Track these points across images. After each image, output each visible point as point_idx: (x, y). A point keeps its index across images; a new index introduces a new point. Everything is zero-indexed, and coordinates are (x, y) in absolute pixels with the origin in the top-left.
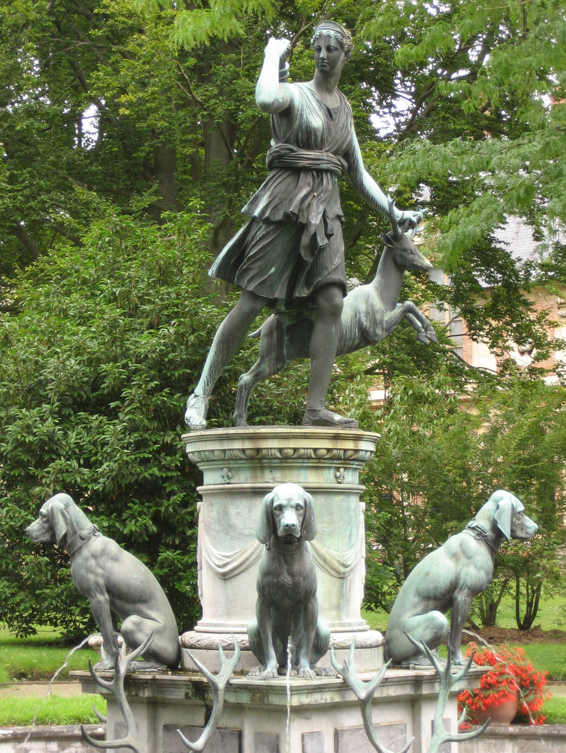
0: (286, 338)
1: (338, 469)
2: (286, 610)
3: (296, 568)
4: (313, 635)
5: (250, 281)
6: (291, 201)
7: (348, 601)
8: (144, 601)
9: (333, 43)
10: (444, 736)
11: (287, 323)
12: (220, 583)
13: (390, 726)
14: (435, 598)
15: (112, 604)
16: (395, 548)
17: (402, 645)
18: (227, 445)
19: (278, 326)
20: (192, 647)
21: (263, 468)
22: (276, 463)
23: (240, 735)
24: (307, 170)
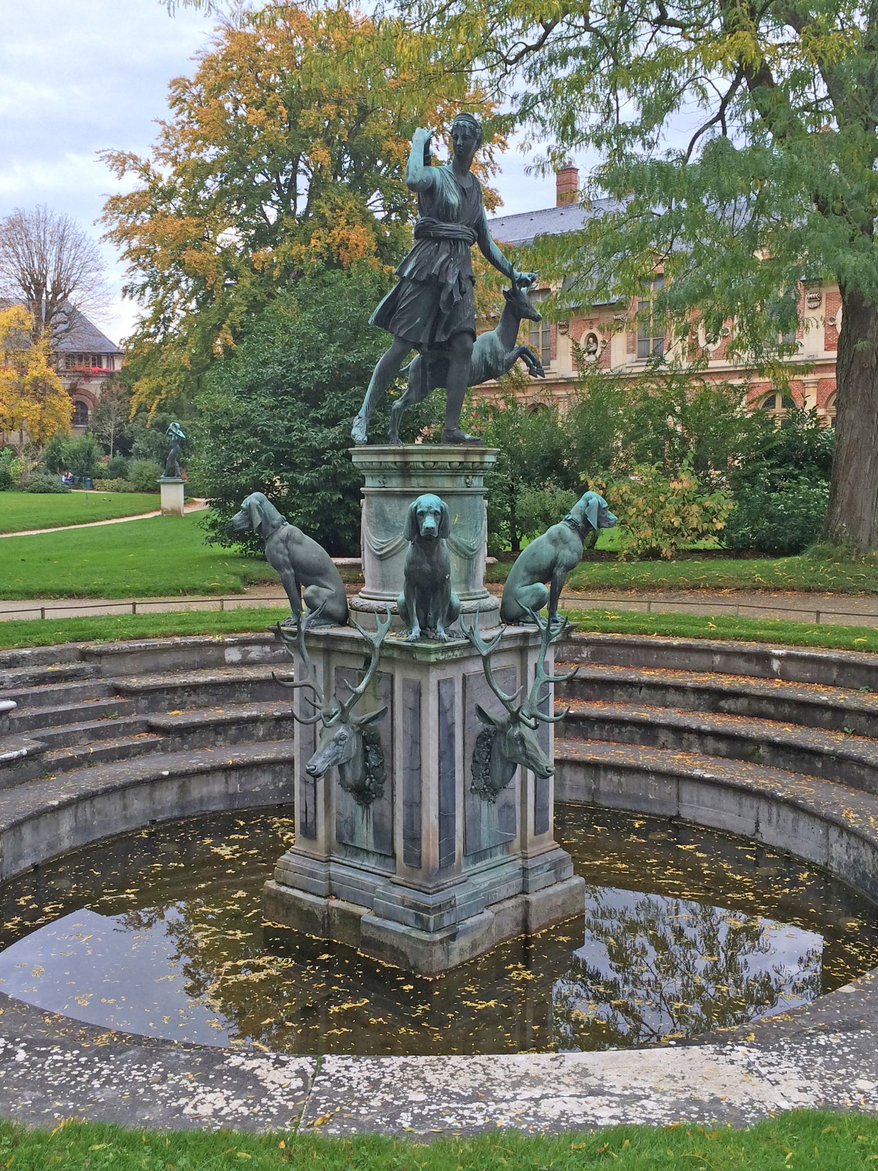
0: (429, 373)
1: (467, 477)
2: (427, 593)
3: (435, 559)
4: (447, 609)
6: (433, 265)
9: (467, 132)
10: (544, 677)
11: (429, 361)
12: (377, 562)
14: (540, 573)
15: (296, 576)
16: (510, 527)
17: (514, 609)
18: (383, 458)
19: (422, 364)
20: (357, 609)
21: (410, 476)
22: (420, 472)
23: (392, 677)
24: (445, 239)
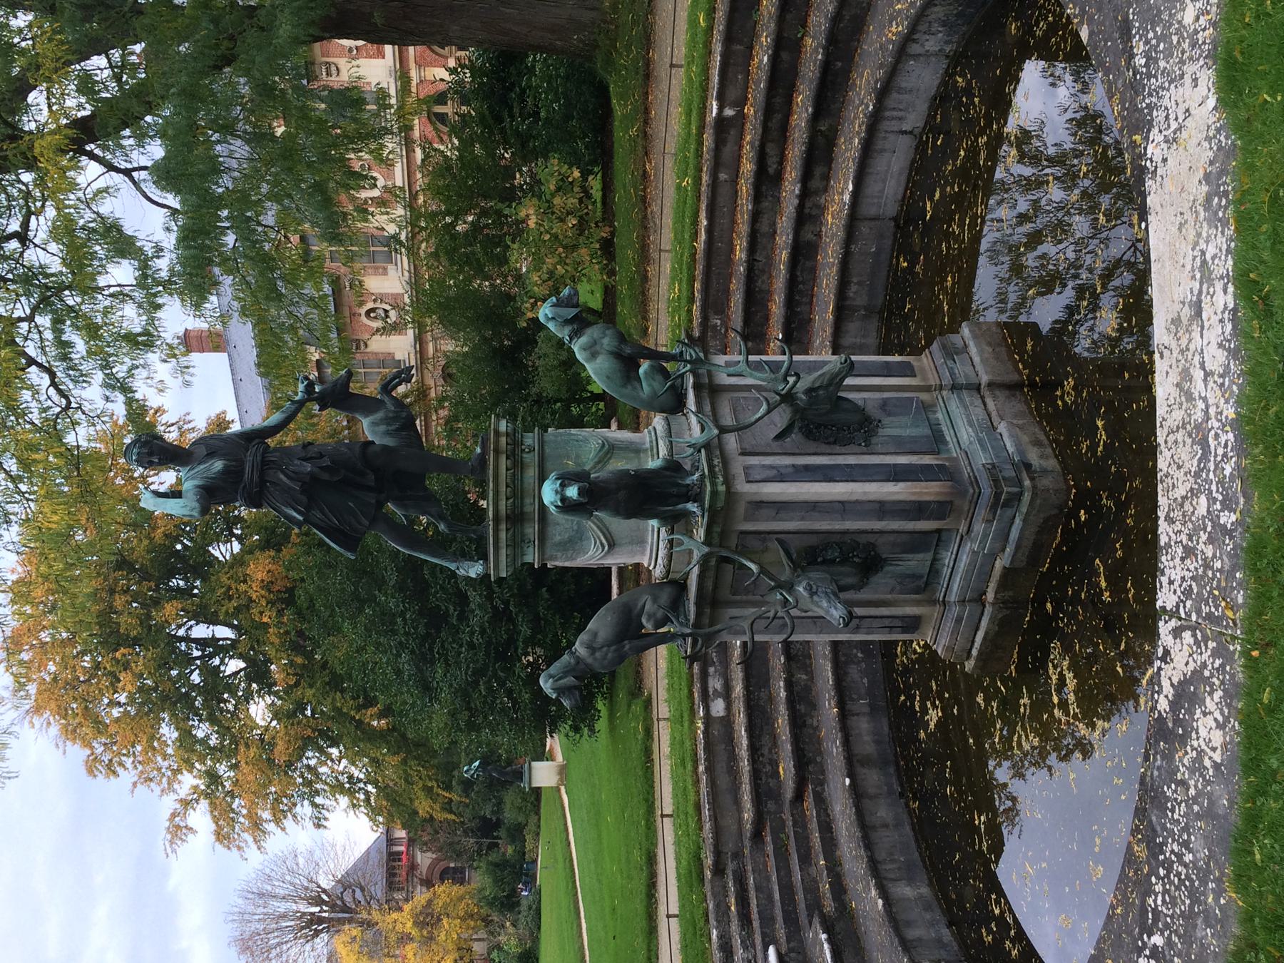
1: (523, 451)
2: (651, 494)
5: (360, 524)
6: (290, 488)
7: (632, 443)
8: (630, 611)
12: (617, 549)
13: (735, 410)
18: (503, 543)
19: (399, 502)
20: (668, 572)
21: (522, 513)
23: (742, 533)
